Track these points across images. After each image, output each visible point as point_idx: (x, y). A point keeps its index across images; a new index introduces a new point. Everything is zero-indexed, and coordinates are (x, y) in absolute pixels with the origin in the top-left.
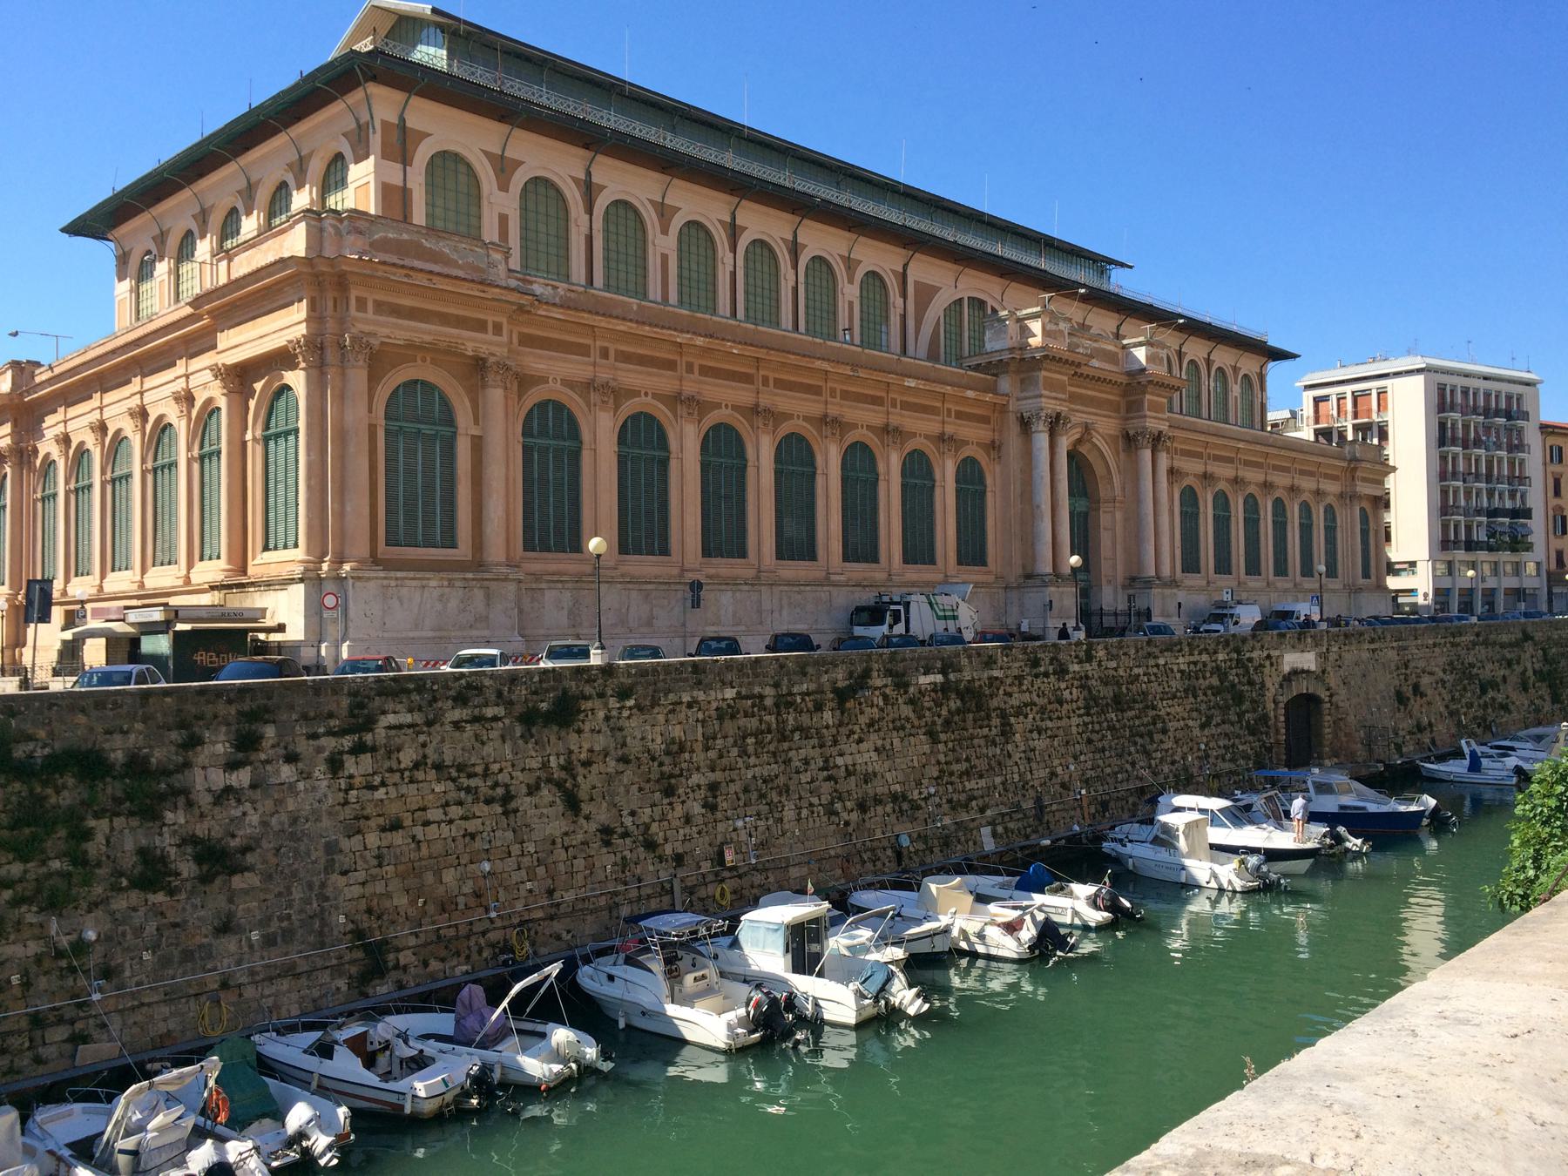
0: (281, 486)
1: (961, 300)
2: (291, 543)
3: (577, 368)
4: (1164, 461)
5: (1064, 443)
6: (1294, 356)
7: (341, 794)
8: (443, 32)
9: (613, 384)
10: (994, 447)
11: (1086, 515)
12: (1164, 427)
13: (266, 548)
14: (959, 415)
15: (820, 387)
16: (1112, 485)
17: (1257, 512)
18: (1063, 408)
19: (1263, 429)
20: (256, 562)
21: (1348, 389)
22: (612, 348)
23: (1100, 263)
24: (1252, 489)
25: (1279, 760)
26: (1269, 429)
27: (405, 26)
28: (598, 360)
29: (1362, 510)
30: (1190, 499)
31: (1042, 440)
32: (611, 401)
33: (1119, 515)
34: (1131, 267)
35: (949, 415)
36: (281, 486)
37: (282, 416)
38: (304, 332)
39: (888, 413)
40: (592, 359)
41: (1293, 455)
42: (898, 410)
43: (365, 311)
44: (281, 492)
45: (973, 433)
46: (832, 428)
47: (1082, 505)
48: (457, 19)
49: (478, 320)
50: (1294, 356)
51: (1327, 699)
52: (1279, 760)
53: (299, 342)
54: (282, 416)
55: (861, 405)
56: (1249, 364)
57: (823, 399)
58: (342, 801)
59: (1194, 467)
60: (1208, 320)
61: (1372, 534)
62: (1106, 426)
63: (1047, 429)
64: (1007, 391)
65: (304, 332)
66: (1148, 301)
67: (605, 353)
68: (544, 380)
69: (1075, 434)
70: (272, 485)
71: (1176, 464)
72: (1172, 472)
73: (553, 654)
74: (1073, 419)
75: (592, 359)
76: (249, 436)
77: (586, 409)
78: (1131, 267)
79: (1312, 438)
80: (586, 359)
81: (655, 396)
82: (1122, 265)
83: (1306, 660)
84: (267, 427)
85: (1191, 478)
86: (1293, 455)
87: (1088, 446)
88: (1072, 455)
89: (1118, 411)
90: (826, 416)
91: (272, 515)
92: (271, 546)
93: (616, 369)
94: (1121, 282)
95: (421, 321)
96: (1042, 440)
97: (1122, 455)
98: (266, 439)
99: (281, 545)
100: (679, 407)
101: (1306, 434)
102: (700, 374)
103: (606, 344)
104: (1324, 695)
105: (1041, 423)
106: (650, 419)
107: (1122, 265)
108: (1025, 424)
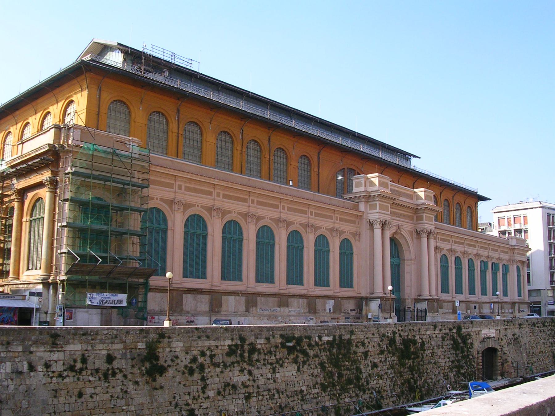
0: (36, 242)
1: (344, 168)
2: (38, 267)
3: (274, 214)
4: (433, 244)
5: (388, 235)
6: (489, 199)
7: (49, 379)
8: (122, 52)
9: (183, 201)
10: (357, 235)
11: (398, 266)
12: (432, 228)
13: (28, 269)
14: (341, 220)
15: (332, 216)
16: (409, 253)
17: (473, 266)
18: (388, 218)
19: (477, 230)
20: (24, 275)
21: (512, 214)
22: (256, 200)
23: (406, 156)
24: (471, 257)
25: (478, 376)
26: (480, 230)
27: (105, 49)
28: (216, 197)
29: (518, 267)
30: (444, 259)
31: (378, 232)
32: (220, 215)
33: (413, 266)
34: (420, 158)
35: (312, 215)
36: (36, 242)
37: (38, 212)
38: (50, 175)
39: (437, 242)
40: (174, 190)
41: (477, 239)
42: (313, 216)
43: (285, 210)
44: (36, 245)
45: (348, 228)
46: (179, 205)
47: (396, 261)
48: (128, 47)
49: (209, 191)
50: (489, 199)
51: (500, 350)
52: (478, 376)
53: (47, 180)
54: (38, 212)
55: (297, 214)
56: (470, 201)
57: (279, 210)
58: (50, 382)
59: (445, 246)
60: (452, 182)
61: (522, 277)
62: (407, 227)
63: (380, 227)
64: (363, 211)
65: (50, 175)
66: (427, 173)
67: (180, 187)
68: (264, 218)
69: (393, 230)
70: (32, 242)
71: (439, 245)
72: (436, 248)
73: (41, 323)
74: (392, 223)
75: (213, 197)
76: (24, 220)
77: (210, 218)
78: (420, 158)
79: (498, 236)
80: (172, 190)
81: (202, 207)
82: (415, 156)
83: (492, 332)
84: (31, 216)
85: (445, 251)
86: (477, 239)
87: (399, 235)
88: (392, 240)
89: (412, 219)
90: (280, 218)
91: (31, 255)
92: (30, 268)
93: (185, 194)
94: (415, 164)
95: (265, 206)
96: (378, 232)
97: (414, 240)
98: (31, 221)
99: (34, 268)
100: (213, 212)
101: (495, 233)
102: (315, 216)
103: (220, 191)
104: (499, 348)
105: (425, 234)
106: (199, 217)
107: (415, 156)
108: (371, 224)
